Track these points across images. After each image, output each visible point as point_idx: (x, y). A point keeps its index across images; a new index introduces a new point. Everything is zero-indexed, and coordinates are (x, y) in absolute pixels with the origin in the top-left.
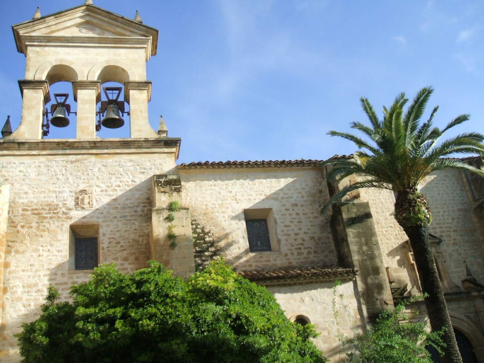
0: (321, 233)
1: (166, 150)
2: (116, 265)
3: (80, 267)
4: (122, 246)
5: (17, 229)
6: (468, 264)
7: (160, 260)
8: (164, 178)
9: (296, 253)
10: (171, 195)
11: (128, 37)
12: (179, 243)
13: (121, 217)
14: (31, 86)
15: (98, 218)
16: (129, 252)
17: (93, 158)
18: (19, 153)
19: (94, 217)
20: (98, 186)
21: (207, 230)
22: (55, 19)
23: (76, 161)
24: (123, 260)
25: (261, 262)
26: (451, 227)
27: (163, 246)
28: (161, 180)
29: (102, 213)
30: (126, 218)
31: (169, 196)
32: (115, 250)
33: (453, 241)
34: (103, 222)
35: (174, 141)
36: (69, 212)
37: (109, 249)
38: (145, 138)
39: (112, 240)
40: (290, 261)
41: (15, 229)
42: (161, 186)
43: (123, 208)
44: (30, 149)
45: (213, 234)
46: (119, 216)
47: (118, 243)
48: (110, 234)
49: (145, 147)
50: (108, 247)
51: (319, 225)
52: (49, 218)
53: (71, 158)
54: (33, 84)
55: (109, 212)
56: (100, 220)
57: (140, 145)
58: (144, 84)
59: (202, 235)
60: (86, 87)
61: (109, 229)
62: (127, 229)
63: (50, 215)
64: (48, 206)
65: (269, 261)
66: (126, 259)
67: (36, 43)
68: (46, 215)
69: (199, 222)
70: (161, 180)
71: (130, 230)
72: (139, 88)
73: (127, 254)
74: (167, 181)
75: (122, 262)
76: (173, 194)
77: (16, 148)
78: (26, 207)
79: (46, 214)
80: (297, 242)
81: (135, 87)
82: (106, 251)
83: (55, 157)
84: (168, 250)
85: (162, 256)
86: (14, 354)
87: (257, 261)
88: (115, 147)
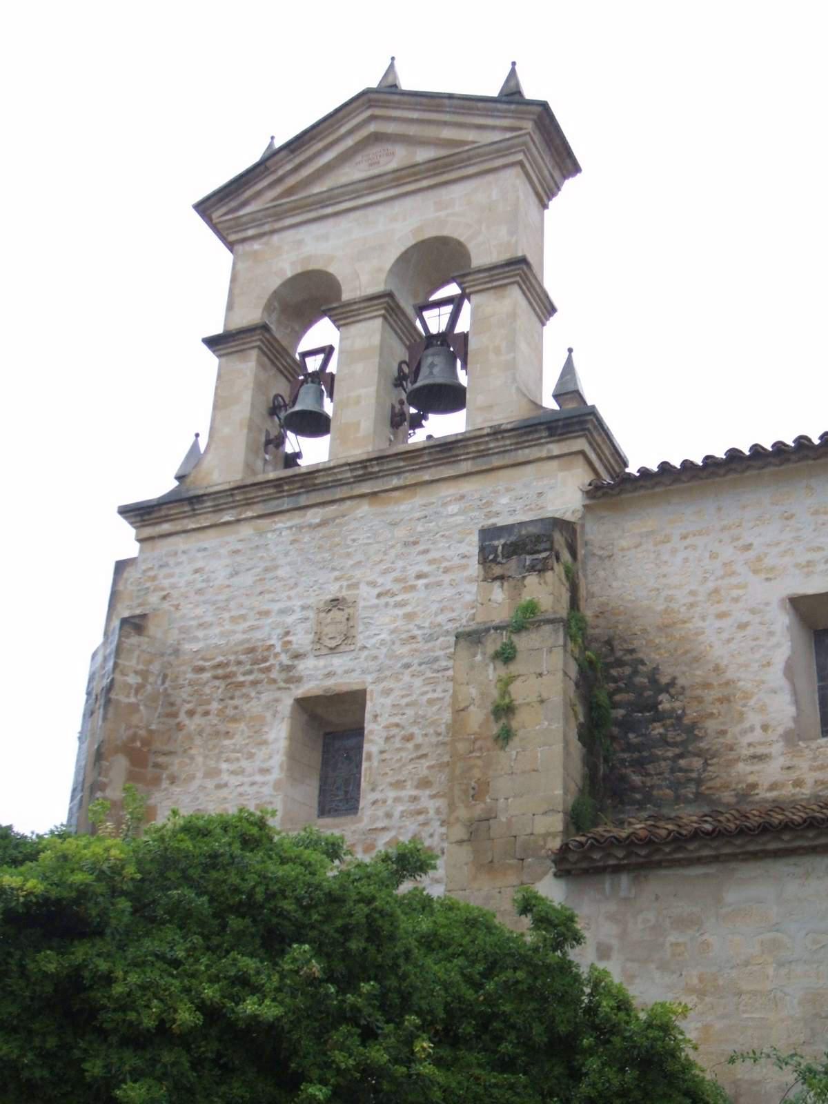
1: (556, 449)
2: (397, 800)
3: (329, 812)
4: (418, 747)
5: (178, 720)
7: (465, 781)
10: (520, 583)
12: (524, 727)
13: (420, 665)
14: (232, 347)
15: (363, 672)
16: (433, 762)
17: (364, 508)
18: (194, 526)
19: (353, 670)
20: (373, 584)
22: (292, 156)
23: (323, 523)
24: (417, 787)
27: (474, 741)
28: (496, 543)
29: (375, 658)
30: (435, 666)
32: (400, 760)
34: (377, 681)
35: (575, 420)
36: (296, 662)
37: (385, 756)
38: (491, 427)
39: (395, 731)
41: (172, 722)
42: (494, 560)
43: (430, 638)
44: (218, 510)
45: (683, 688)
46: (416, 662)
47: (409, 738)
48: (390, 716)
49: (496, 450)
50: (382, 752)
52: (247, 684)
53: (314, 516)
54: (234, 341)
55: (391, 656)
56: (369, 678)
57: (482, 447)
58: (507, 269)
59: (650, 693)
60: (359, 315)
61: (388, 701)
62: (435, 695)
63: (251, 678)
64: (249, 653)
66: (424, 783)
67: (250, 233)
68: (241, 679)
69: (641, 655)
70: (496, 543)
71: (442, 699)
72: (495, 284)
73: (430, 767)
74: (512, 543)
75: (414, 792)
76: (527, 581)
77: (187, 514)
78: (201, 663)
79: (244, 674)
81: (481, 284)
82: (375, 763)
83: (274, 522)
84: (488, 750)
85: (470, 768)
86: (55, 1049)
88: (417, 467)
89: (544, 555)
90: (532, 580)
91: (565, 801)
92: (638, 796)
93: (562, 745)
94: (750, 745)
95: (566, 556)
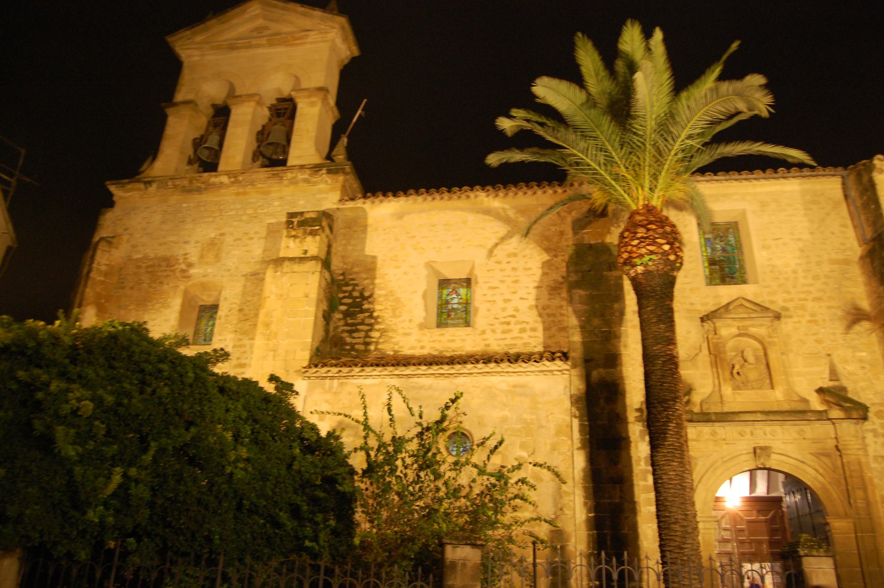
0: (550, 299)
6: (836, 360)
8: (299, 217)
9: (499, 331)
11: (216, 44)
21: (366, 294)
25: (440, 341)
26: (809, 292)
28: (293, 220)
31: (301, 242)
33: (808, 318)
40: (487, 342)
51: (548, 286)
65: (453, 341)
80: (505, 314)
87: (434, 341)
89: (317, 228)
90: (309, 239)
91: (312, 345)
92: (348, 347)
93: (313, 318)
94: (403, 328)
95: (327, 231)
